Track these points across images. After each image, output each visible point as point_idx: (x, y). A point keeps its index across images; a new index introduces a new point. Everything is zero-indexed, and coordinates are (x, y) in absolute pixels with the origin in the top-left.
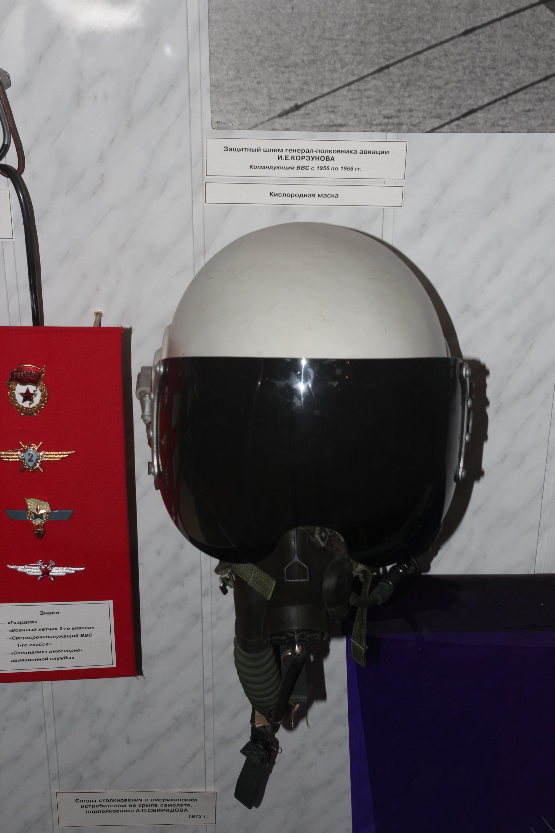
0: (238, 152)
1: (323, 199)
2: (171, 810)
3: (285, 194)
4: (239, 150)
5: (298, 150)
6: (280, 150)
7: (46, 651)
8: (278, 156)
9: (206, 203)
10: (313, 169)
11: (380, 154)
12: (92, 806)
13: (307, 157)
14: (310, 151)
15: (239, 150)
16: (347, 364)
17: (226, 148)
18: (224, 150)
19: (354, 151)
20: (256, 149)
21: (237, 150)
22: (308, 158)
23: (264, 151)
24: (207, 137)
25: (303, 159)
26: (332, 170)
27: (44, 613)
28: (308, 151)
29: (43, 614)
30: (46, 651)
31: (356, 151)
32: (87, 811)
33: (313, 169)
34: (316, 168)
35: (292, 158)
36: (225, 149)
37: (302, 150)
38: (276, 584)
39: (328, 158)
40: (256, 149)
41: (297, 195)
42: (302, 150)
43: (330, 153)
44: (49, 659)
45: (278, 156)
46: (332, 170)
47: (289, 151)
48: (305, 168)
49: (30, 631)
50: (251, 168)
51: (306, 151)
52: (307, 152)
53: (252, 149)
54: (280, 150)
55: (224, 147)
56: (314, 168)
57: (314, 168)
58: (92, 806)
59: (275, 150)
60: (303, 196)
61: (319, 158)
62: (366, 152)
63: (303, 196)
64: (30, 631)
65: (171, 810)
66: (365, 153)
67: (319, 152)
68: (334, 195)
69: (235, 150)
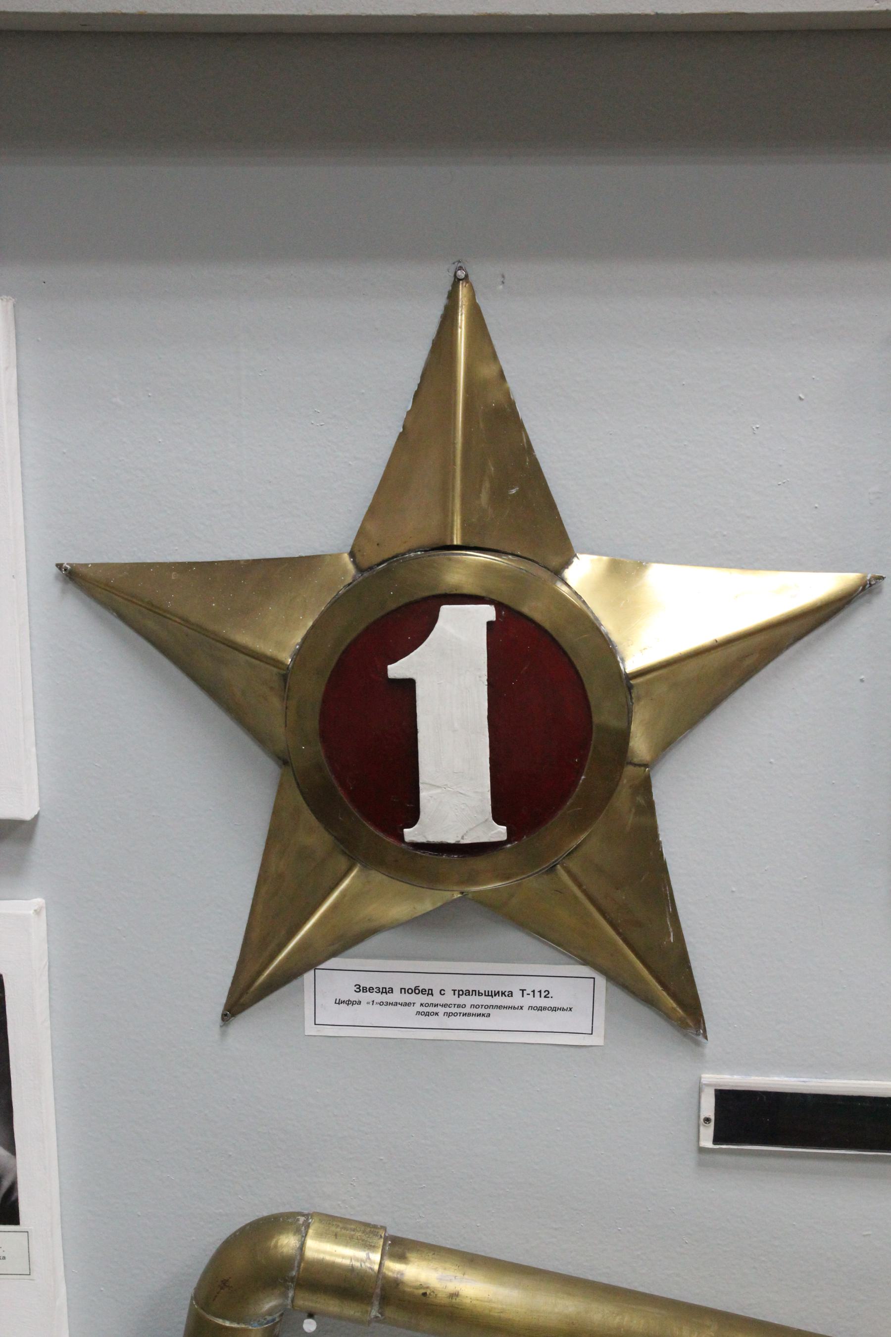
1: (501, 989)
2: (383, 990)
4: (493, 994)
5: (422, 990)
7: (414, 1003)
10: (444, 994)
11: (492, 997)
12: (459, 991)
13: (376, 988)
14: (471, 994)
15: (493, 994)
18: (355, 991)
19: (508, 992)
21: (490, 994)
22: (357, 988)
23: (335, 1003)
25: (460, 996)
26: (529, 1009)
27: (361, 988)
28: (469, 993)
29: (379, 992)
30: (414, 1003)
31: (392, 989)
32: (401, 989)
33: (442, 992)
34: (436, 992)
35: (511, 994)
36: (355, 988)
39: (365, 988)
40: (485, 991)
43: (502, 996)
46: (529, 1009)
48: (368, 990)
49: (563, 1010)
50: (503, 995)
51: (464, 992)
52: (467, 994)
53: (479, 991)
56: (444, 991)
57: (444, 991)
58: (459, 991)
59: (424, 990)
62: (366, 990)
64: (563, 1010)
65: (383, 990)
66: (365, 991)
67: (405, 993)
68: (505, 991)
69: (487, 994)
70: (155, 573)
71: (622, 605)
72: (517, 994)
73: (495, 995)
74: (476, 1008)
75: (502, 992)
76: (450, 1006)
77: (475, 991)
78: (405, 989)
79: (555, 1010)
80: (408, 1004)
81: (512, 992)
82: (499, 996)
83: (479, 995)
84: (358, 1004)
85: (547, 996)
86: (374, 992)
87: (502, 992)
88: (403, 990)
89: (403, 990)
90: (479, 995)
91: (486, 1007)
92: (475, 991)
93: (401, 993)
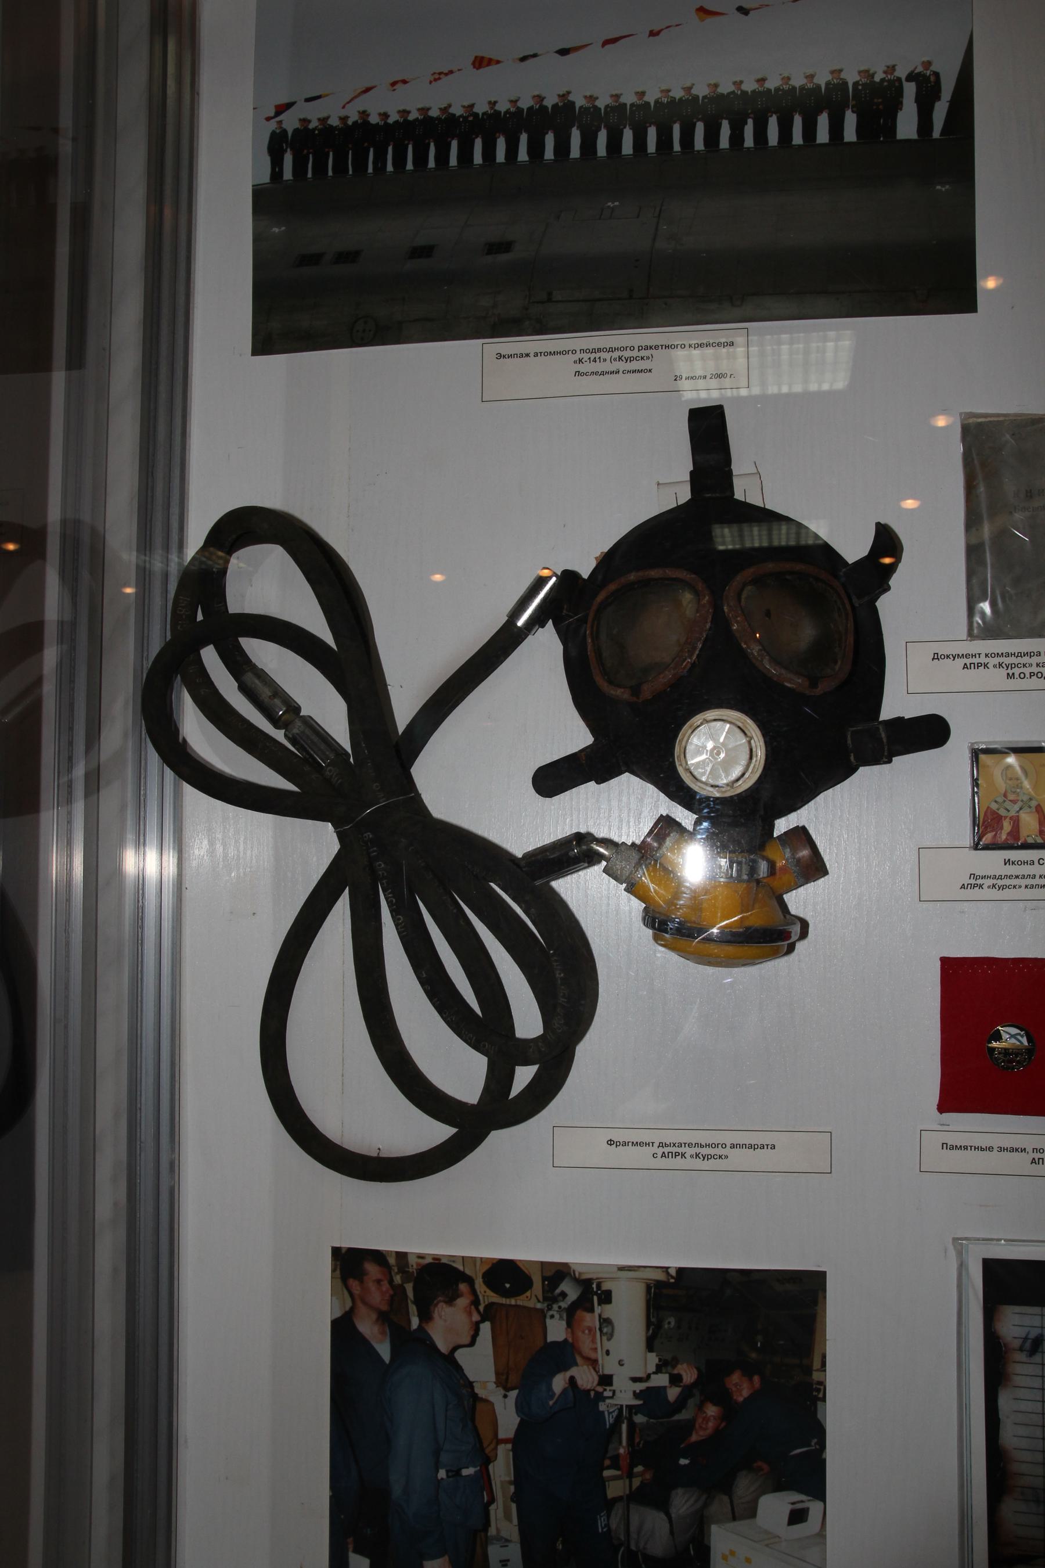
0: (1022, 657)
3: (1037, 1149)
6: (635, 1143)
8: (1005, 860)
9: (483, 344)
16: (936, 414)
17: (499, 355)
20: (986, 1147)
23: (1043, 1159)
24: (833, 1133)
32: (1034, 1149)
33: (655, 1156)
35: (690, 346)
37: (724, 343)
38: (831, 394)
40: (986, 1147)
41: (605, 350)
42: (724, 343)
44: (621, 372)
45: (1005, 860)
47: (689, 1145)
51: (621, 1143)
54: (635, 1143)
55: (497, 354)
60: (614, 350)
61: (709, 1145)
63: (614, 350)
65: (1018, 654)
70: (250, 871)
71: (619, 692)
72: (983, 656)
73: (1024, 656)
74: (621, 350)
75: (984, 663)
76: (638, 358)
77: (698, 1144)
78: (740, 1145)
79: (603, 375)
80: (671, 346)
81: (774, 1145)
82: (1009, 864)
83: (981, 1150)
84: (645, 349)
85: (770, 1546)
86: (1029, 1149)
87: (984, 663)
88: (582, 351)
89: (582, 351)
90: (981, 1150)
91: (546, 354)
92: (698, 1144)
93: (943, 1149)
